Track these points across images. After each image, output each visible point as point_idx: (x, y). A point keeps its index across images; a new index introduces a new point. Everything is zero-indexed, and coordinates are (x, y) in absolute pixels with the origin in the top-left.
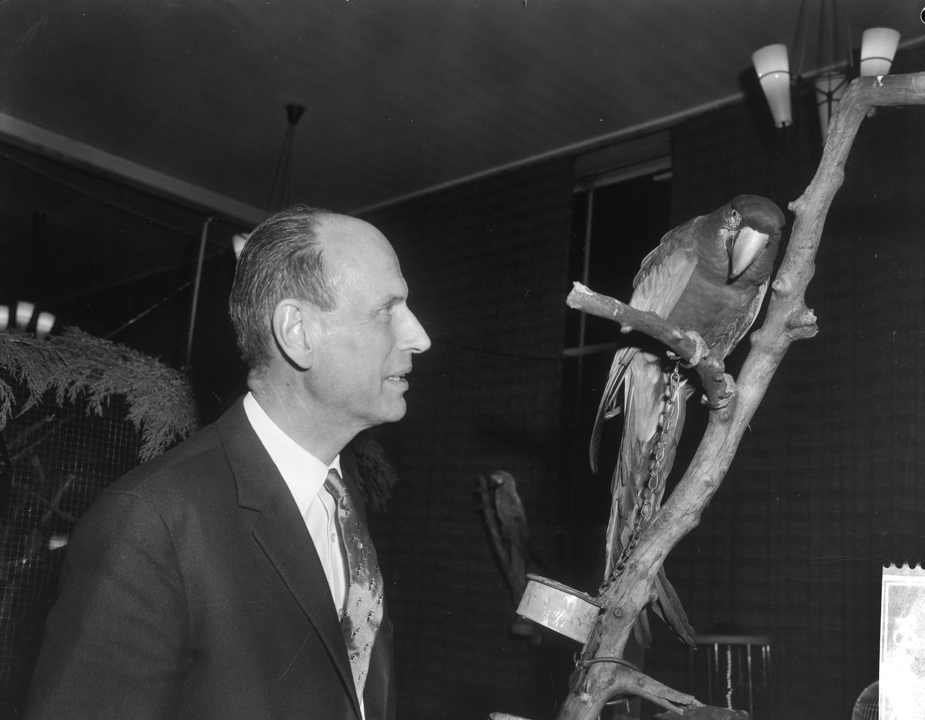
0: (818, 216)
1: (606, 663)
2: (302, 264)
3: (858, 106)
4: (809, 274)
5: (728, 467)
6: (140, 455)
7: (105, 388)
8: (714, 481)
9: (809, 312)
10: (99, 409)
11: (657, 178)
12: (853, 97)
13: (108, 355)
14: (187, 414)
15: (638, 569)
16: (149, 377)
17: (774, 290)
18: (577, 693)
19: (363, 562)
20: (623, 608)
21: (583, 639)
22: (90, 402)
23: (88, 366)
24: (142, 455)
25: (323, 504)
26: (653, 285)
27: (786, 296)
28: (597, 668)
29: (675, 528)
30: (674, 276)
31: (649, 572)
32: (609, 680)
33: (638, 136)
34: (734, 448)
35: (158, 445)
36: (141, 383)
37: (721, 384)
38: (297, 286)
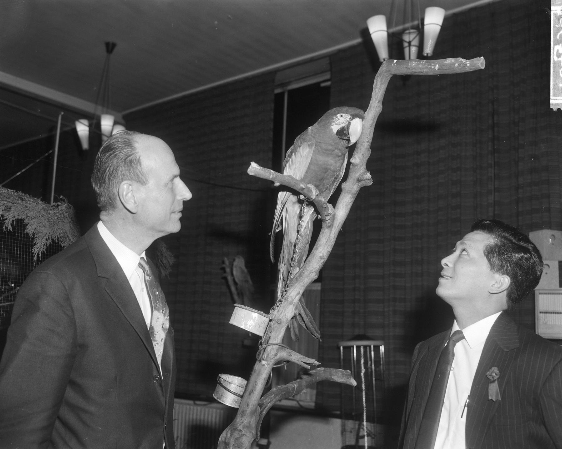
0: (370, 127)
1: (273, 346)
2: (131, 164)
3: (386, 74)
4: (368, 154)
5: (331, 249)
6: (33, 251)
7: (13, 216)
8: (324, 256)
9: (368, 173)
10: (10, 228)
11: (323, 85)
12: (383, 70)
13: (13, 197)
14: (57, 229)
15: (288, 300)
16: (36, 209)
17: (351, 163)
18: (260, 361)
19: (158, 300)
20: (281, 319)
21: (261, 334)
22: (5, 224)
23: (3, 204)
24: (34, 251)
25: (138, 274)
26: (294, 163)
27: (357, 165)
28: (269, 349)
29: (306, 280)
30: (303, 157)
31: (294, 301)
32: (275, 354)
33: (312, 60)
34: (334, 240)
35: (43, 246)
36: (32, 213)
37: (326, 209)
38: (129, 174)
